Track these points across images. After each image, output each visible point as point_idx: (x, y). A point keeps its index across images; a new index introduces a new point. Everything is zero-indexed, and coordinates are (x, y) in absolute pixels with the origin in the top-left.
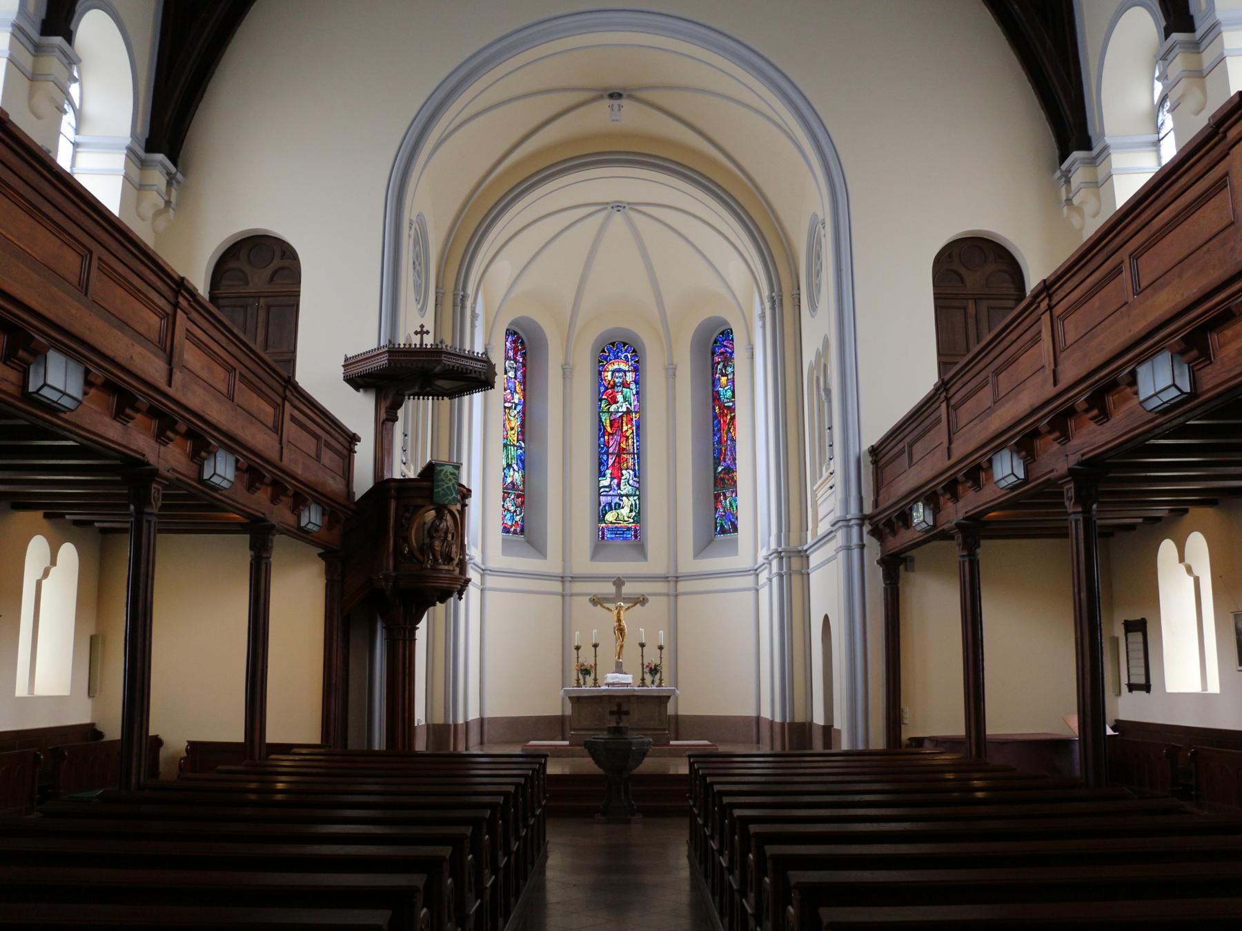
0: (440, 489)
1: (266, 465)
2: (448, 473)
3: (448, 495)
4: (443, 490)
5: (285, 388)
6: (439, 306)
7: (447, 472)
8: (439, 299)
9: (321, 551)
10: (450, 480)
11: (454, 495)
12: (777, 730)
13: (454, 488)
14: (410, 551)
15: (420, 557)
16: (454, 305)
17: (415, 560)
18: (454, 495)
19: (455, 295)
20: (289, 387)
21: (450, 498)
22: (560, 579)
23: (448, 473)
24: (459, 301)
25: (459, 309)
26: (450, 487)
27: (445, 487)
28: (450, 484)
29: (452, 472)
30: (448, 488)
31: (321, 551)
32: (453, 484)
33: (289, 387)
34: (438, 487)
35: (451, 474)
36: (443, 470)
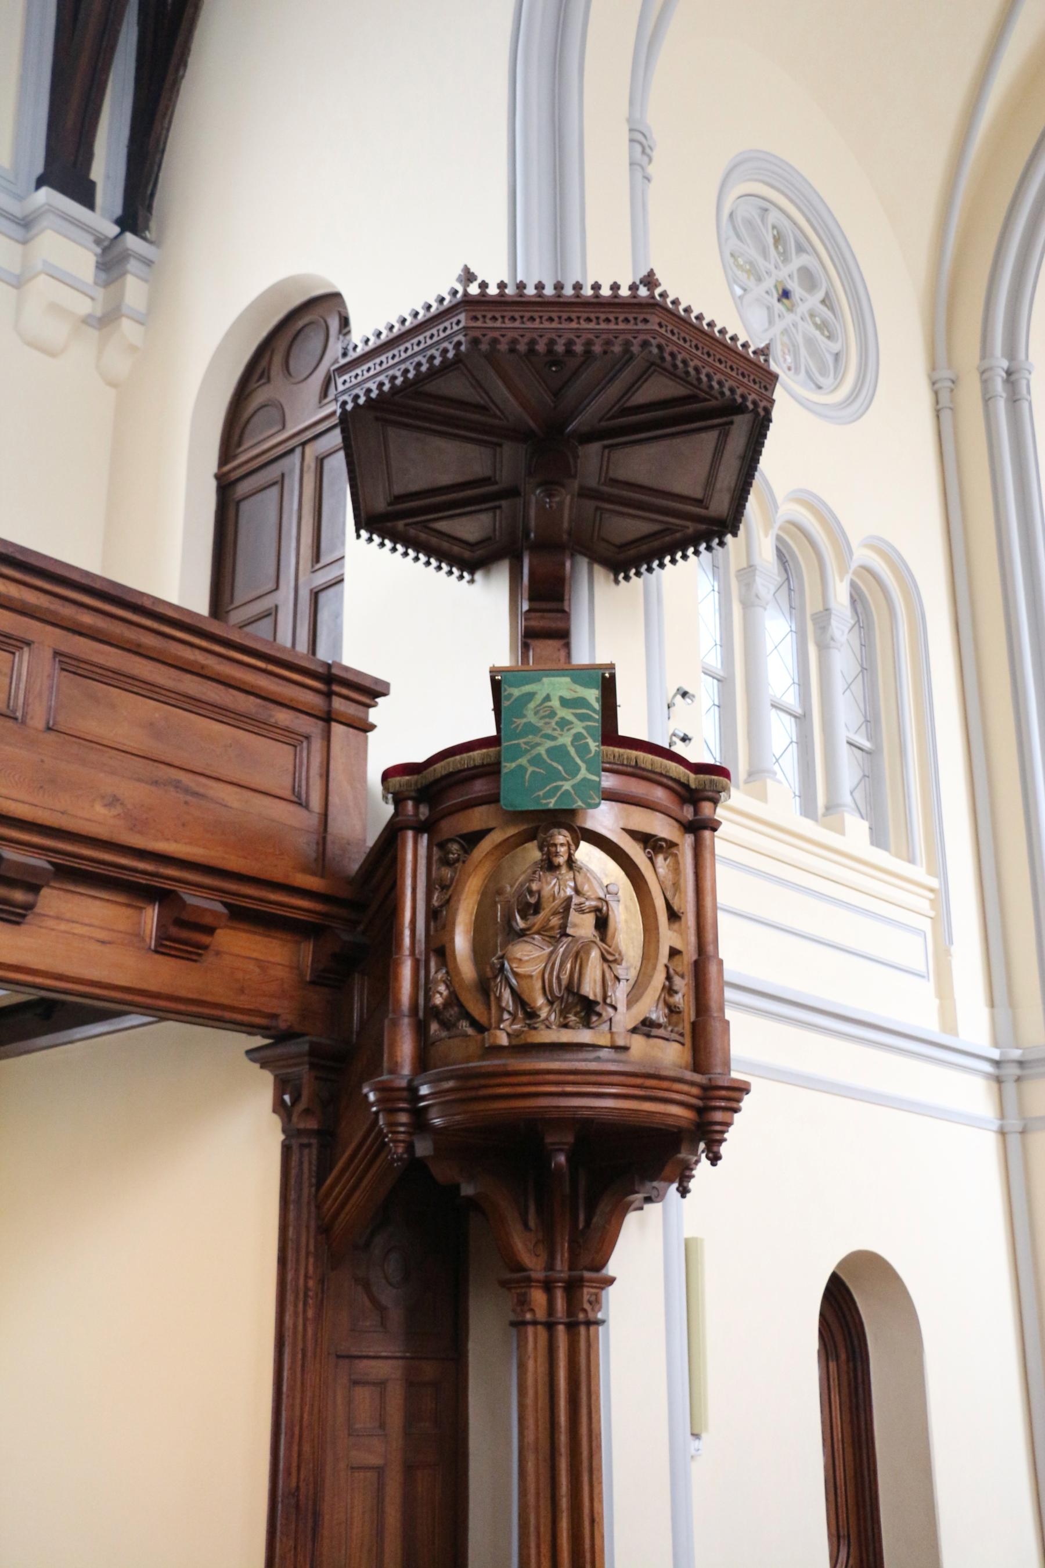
0: (523, 761)
1: (532, 1529)
2: (555, 703)
3: (558, 776)
4: (536, 760)
5: (329, 695)
6: (946, 415)
7: (548, 698)
8: (945, 397)
9: (258, 1041)
10: (564, 724)
11: (583, 773)
12: (538, 605)
13: (582, 750)
14: (454, 999)
15: (476, 1009)
16: (987, 399)
17: (464, 1025)
18: (583, 773)
19: (985, 374)
20: (336, 688)
21: (567, 786)
22: (988, 1068)
23: (555, 703)
24: (999, 385)
25: (1001, 406)
26: (562, 748)
27: (542, 750)
28: (566, 739)
29: (568, 695)
30: (559, 753)
31: (258, 1041)
32: (578, 737)
33: (336, 688)
34: (521, 753)
35: (565, 702)
36: (531, 696)
